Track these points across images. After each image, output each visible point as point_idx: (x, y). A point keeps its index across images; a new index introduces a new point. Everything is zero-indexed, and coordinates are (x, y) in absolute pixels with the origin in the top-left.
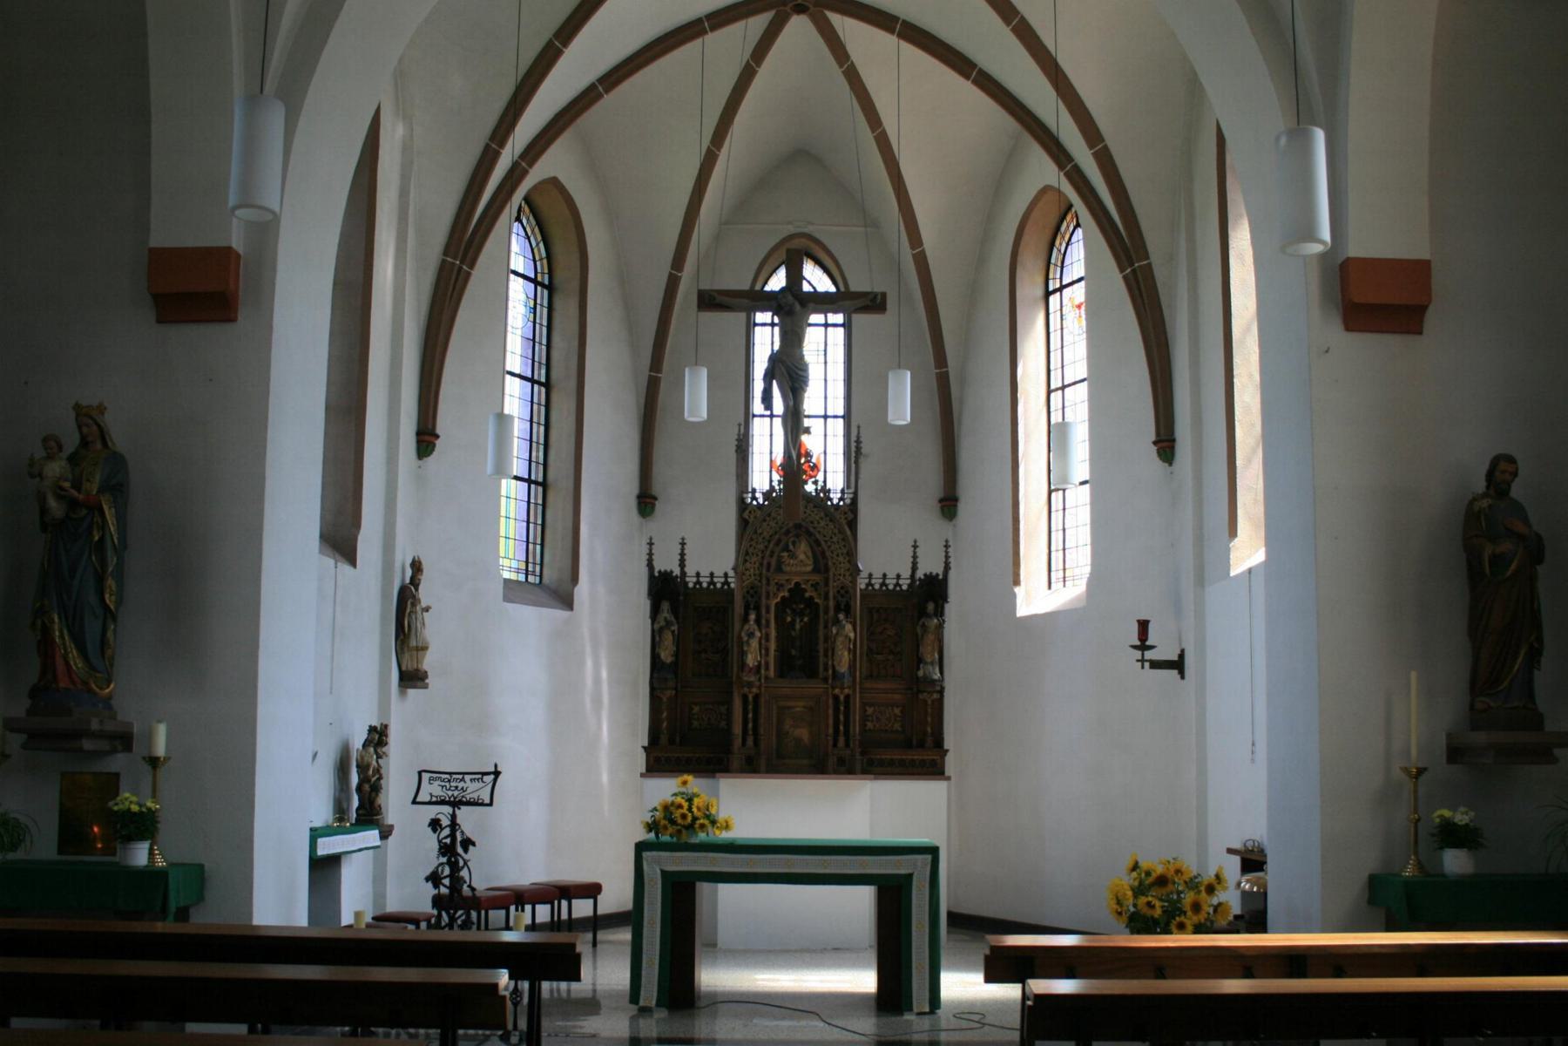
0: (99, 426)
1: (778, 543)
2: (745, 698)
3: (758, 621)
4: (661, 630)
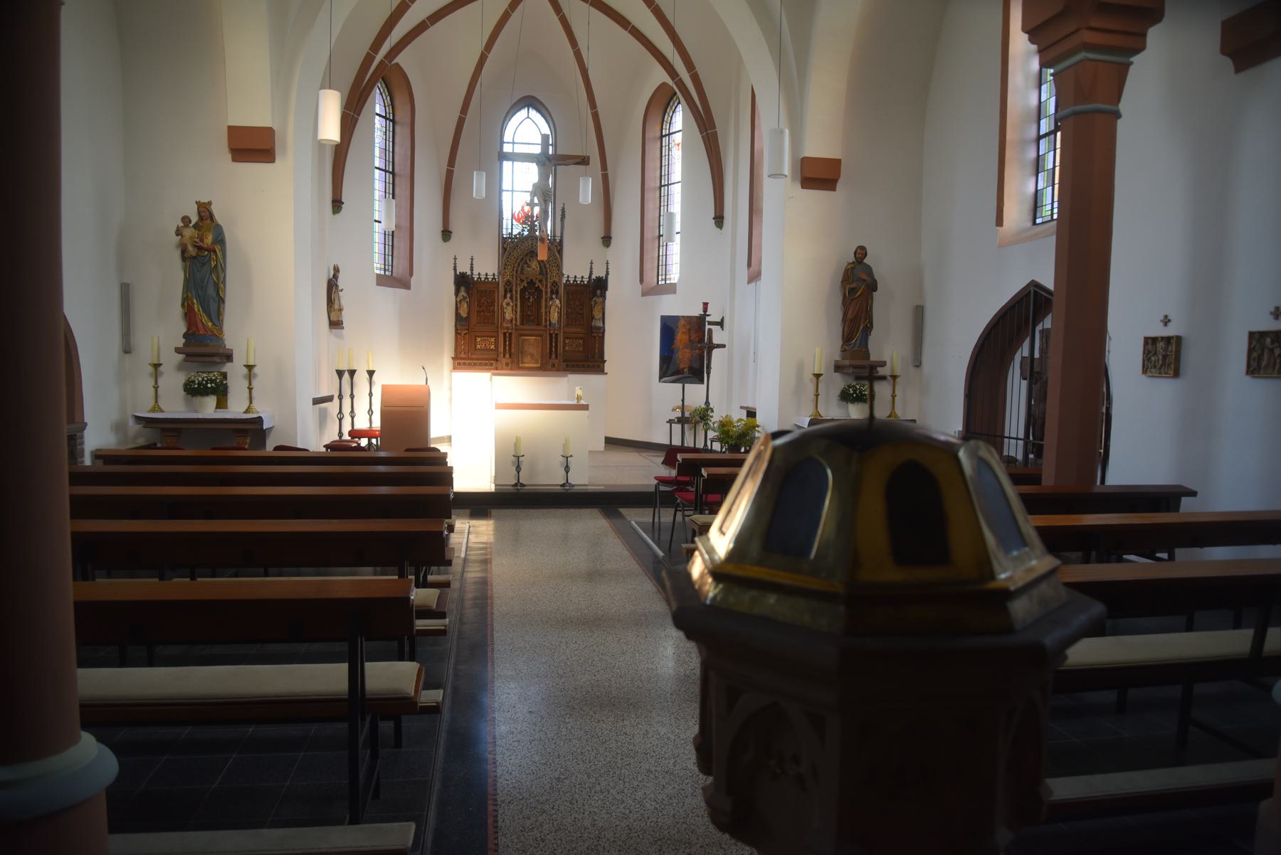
0: (209, 211)
1: (521, 261)
2: (505, 334)
3: (511, 298)
4: (460, 301)
